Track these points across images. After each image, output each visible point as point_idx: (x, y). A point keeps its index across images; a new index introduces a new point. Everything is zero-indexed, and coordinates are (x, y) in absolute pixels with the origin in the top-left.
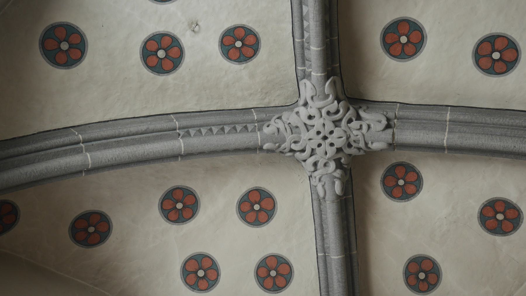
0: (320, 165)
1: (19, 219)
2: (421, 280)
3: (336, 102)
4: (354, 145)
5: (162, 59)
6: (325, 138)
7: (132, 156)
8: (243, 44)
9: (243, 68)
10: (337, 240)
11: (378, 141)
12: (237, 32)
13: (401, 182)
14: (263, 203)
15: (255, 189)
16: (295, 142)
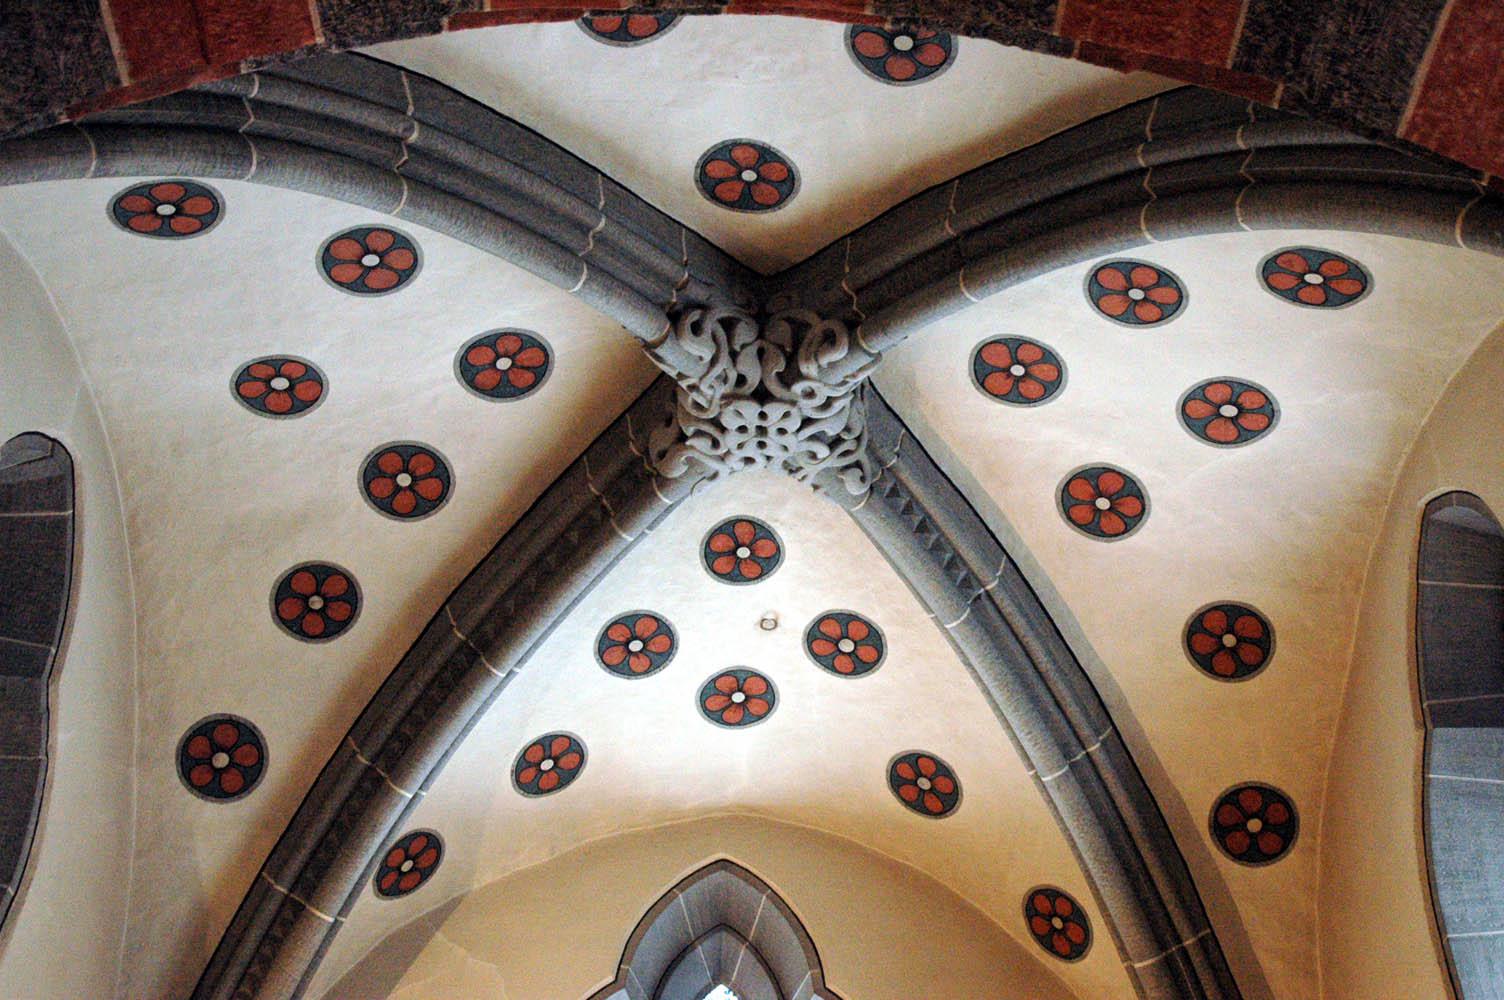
0: (819, 401)
1: (1245, 783)
2: (914, 40)
3: (688, 443)
4: (733, 376)
5: (855, 643)
6: (762, 430)
7: (1010, 705)
8: (739, 546)
9: (778, 524)
10: (937, 310)
11: (690, 354)
12: (727, 569)
13: (749, 176)
14: (1002, 363)
15: (982, 389)
16: (813, 456)
